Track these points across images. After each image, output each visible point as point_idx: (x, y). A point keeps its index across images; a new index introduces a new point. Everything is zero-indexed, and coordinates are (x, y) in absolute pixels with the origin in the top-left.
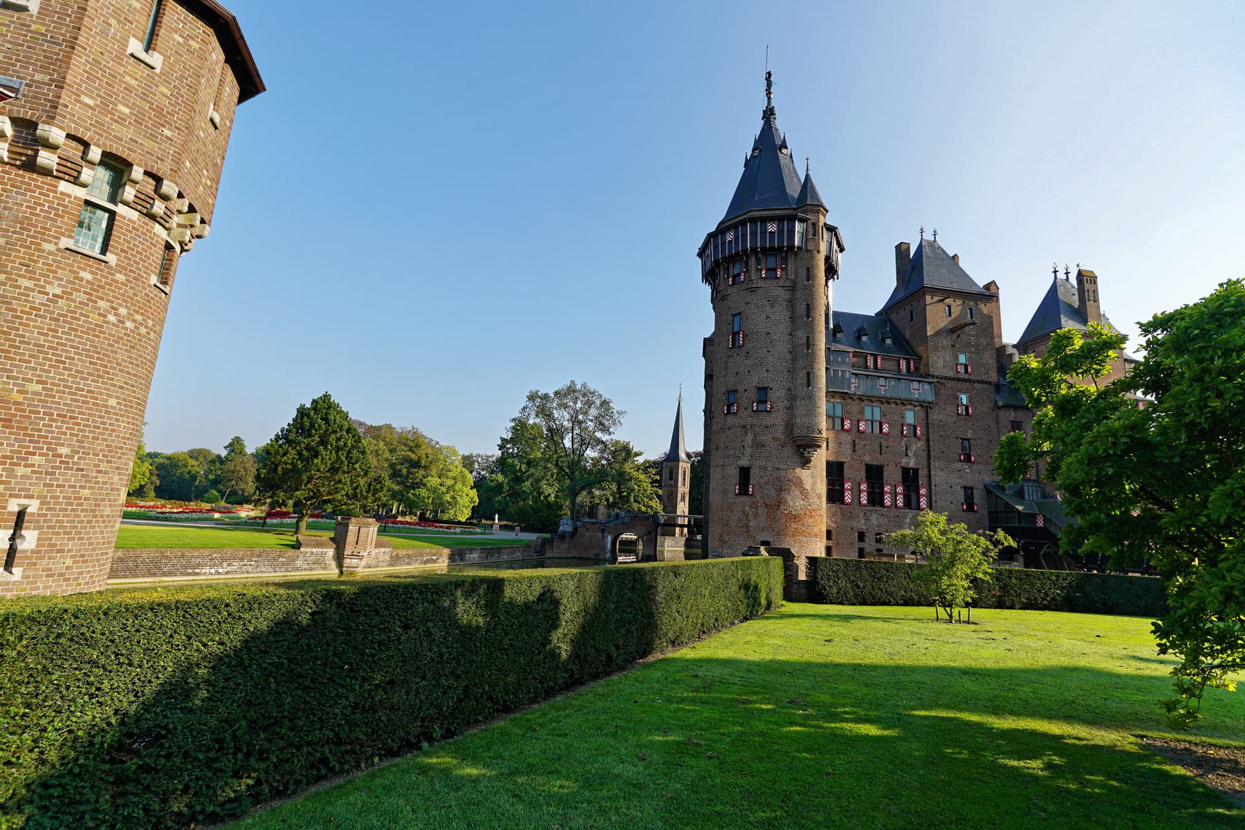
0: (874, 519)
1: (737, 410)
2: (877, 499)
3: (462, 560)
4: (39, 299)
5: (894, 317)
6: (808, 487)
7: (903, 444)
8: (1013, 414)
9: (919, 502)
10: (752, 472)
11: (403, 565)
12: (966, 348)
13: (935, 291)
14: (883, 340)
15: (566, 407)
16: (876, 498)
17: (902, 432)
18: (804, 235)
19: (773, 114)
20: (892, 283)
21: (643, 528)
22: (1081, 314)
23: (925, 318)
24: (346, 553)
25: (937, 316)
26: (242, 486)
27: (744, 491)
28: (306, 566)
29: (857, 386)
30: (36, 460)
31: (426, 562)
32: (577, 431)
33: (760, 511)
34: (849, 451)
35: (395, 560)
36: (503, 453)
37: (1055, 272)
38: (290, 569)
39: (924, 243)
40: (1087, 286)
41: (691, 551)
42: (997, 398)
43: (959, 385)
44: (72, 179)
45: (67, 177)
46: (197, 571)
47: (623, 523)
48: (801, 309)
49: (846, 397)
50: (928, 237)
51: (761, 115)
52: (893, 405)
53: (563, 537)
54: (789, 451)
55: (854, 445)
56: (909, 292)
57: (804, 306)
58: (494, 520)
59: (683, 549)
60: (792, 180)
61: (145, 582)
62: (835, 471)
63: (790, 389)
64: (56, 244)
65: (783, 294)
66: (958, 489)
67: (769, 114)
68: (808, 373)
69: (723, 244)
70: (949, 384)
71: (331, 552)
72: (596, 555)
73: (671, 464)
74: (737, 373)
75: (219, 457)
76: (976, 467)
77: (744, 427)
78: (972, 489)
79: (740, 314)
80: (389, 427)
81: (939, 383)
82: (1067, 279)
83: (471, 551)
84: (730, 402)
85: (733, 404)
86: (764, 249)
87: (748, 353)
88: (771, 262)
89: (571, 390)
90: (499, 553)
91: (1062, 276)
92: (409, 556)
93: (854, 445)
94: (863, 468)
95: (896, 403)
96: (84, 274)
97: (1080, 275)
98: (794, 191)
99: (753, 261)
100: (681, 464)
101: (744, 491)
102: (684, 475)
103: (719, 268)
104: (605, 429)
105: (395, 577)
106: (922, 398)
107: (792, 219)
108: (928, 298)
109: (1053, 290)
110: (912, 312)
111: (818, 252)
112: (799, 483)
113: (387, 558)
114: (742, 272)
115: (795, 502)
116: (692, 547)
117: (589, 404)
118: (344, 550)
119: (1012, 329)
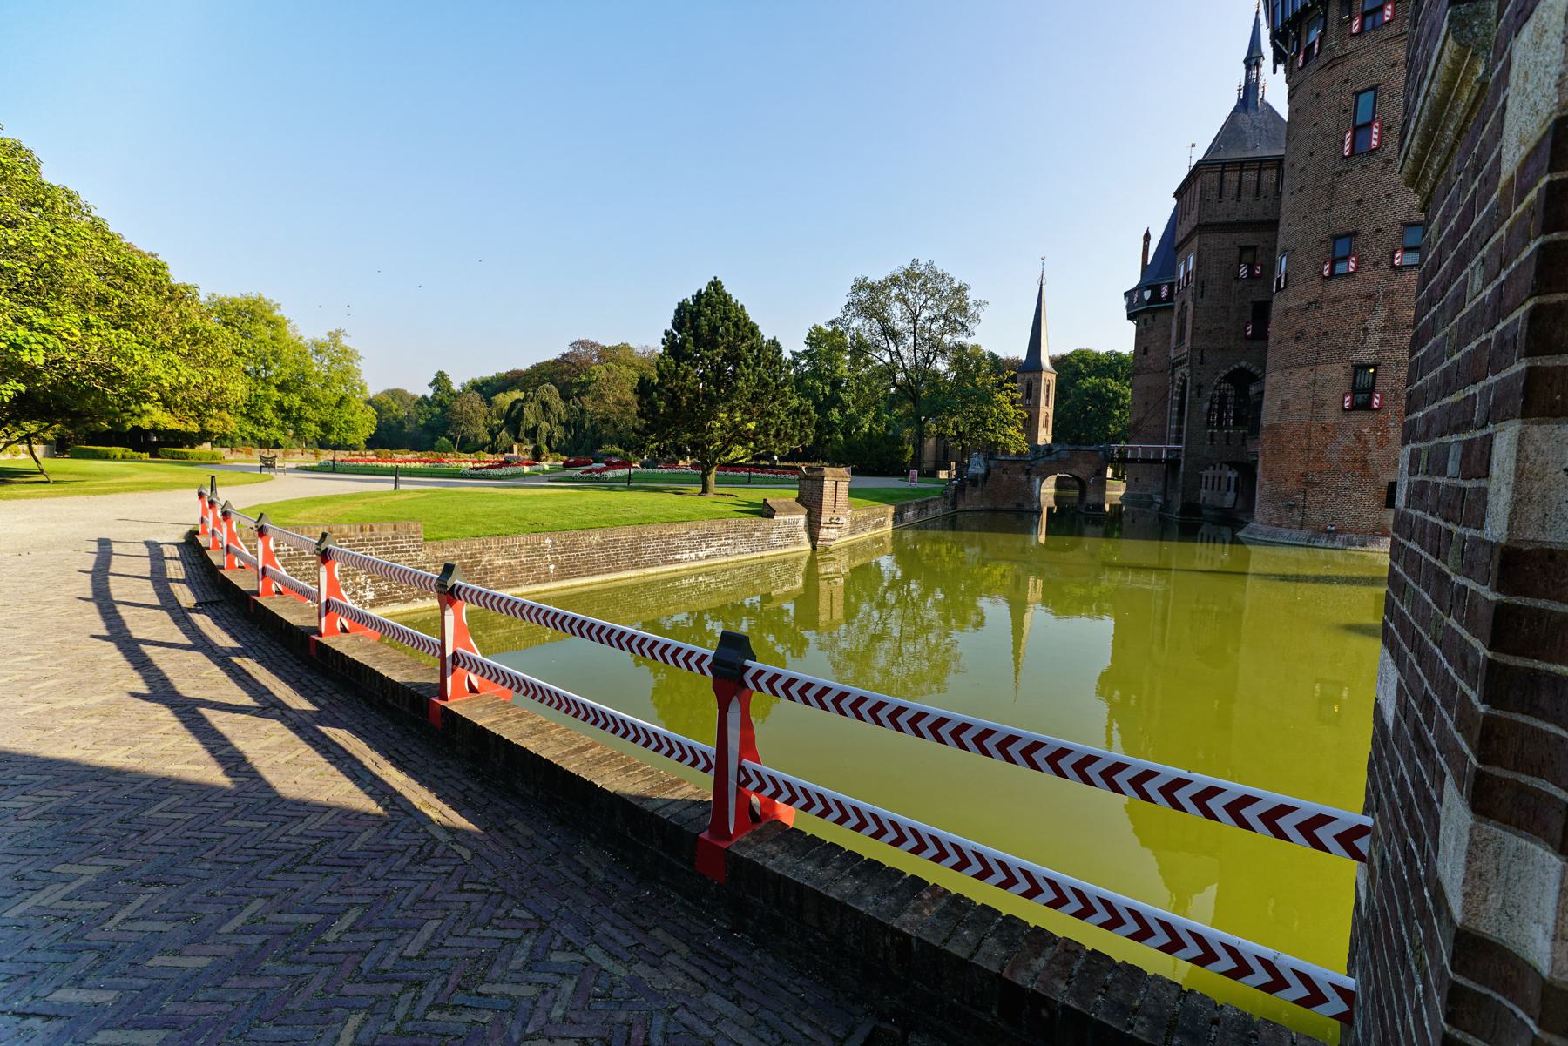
1: (1357, 269)
24: (823, 520)
26: (475, 430)
28: (780, 542)
38: (766, 547)
41: (1064, 493)
46: (678, 557)
47: (1058, 460)
59: (1053, 491)
61: (630, 578)
71: (801, 519)
73: (1029, 376)
74: (1360, 202)
75: (425, 397)
77: (1369, 297)
79: (1374, 88)
80: (626, 347)
84: (1338, 255)
89: (911, 275)
100: (1044, 375)
102: (1048, 391)
105: (71, 473)
116: (1066, 488)
118: (820, 516)
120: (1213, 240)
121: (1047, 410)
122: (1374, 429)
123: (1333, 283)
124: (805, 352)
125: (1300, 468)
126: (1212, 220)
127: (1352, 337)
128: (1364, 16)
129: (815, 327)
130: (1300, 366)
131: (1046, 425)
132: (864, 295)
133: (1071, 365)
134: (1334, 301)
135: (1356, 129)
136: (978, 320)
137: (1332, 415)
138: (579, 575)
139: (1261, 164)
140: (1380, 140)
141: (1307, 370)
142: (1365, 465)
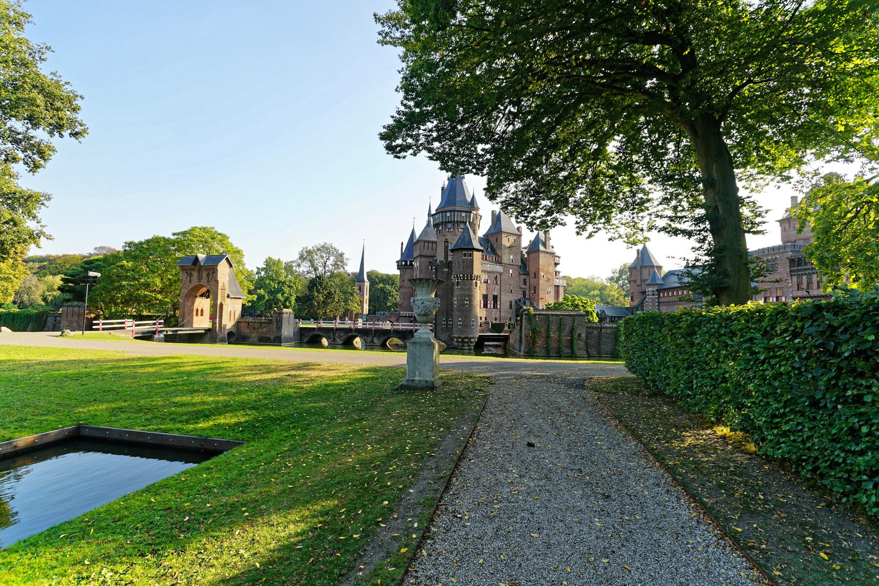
22: (544, 245)
73: (360, 283)
120: (423, 259)
121: (366, 297)
129: (269, 258)
136: (346, 265)
138: (537, 357)
139: (433, 242)
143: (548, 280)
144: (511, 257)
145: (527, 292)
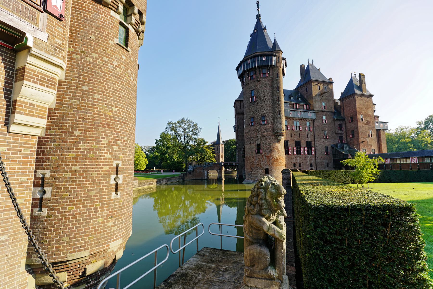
0: (298, 159)
2: (299, 152)
3: (160, 183)
4: (111, 67)
5: (300, 90)
6: (280, 149)
7: (306, 134)
8: (339, 122)
9: (312, 153)
10: (301, 142)
11: (142, 186)
12: (325, 101)
13: (315, 81)
14: (298, 99)
15: (181, 127)
16: (299, 152)
17: (306, 130)
18: (276, 61)
19: (260, 17)
20: (299, 78)
21: (218, 168)
22: (360, 88)
23: (312, 90)
25: (316, 90)
27: (259, 152)
29: (291, 115)
30: (119, 143)
31: (149, 185)
32: (186, 135)
33: (265, 158)
34: (290, 137)
35: (140, 185)
36: (157, 145)
37: (352, 74)
39: (309, 65)
40: (362, 79)
41: (226, 175)
42: (334, 117)
43: (323, 113)
44: (115, 10)
45: (113, 8)
47: (210, 166)
48: (276, 88)
49: (288, 118)
50: (310, 62)
51: (256, 17)
52: (303, 121)
53: (190, 172)
54: (273, 137)
55: (291, 135)
56: (305, 82)
57: (276, 86)
58: (153, 169)
60: (269, 41)
62: (286, 143)
63: (272, 116)
64: (113, 41)
65: (269, 83)
66: (323, 147)
67: (258, 17)
68: (279, 110)
69: (247, 64)
70: (320, 113)
72: (202, 178)
73: (217, 145)
76: (328, 140)
78: (327, 147)
81: (317, 112)
82: (355, 77)
83: (163, 179)
84: (252, 121)
85: (253, 122)
86: (262, 66)
87: (258, 104)
88: (264, 71)
89: (183, 121)
90: (171, 180)
91: (353, 75)
92: (144, 183)
93: (291, 135)
94: (294, 142)
95: (304, 120)
96: (123, 57)
97: (360, 75)
98: (270, 45)
99: (258, 71)
100: (221, 145)
101: (259, 152)
103: (245, 74)
104: (196, 134)
106: (312, 118)
107: (271, 55)
108: (313, 83)
109: (351, 80)
110: (307, 88)
111: (280, 67)
112: (277, 149)
113: (137, 184)
114: (254, 75)
115: (276, 155)
116: (227, 173)
117: (190, 126)
119: (337, 95)
121: (222, 154)
122: (261, 157)
123: (251, 127)
124: (160, 139)
125: (250, 166)
126: (239, 112)
127: (256, 138)
128: (251, 77)
130: (248, 144)
131: (222, 158)
132: (171, 125)
133: (229, 143)
134: (252, 131)
135: (252, 97)
137: (254, 155)
140: (256, 100)
141: (249, 145)
142: (261, 165)
143: (368, 123)
144: (324, 104)
145: (344, 137)
